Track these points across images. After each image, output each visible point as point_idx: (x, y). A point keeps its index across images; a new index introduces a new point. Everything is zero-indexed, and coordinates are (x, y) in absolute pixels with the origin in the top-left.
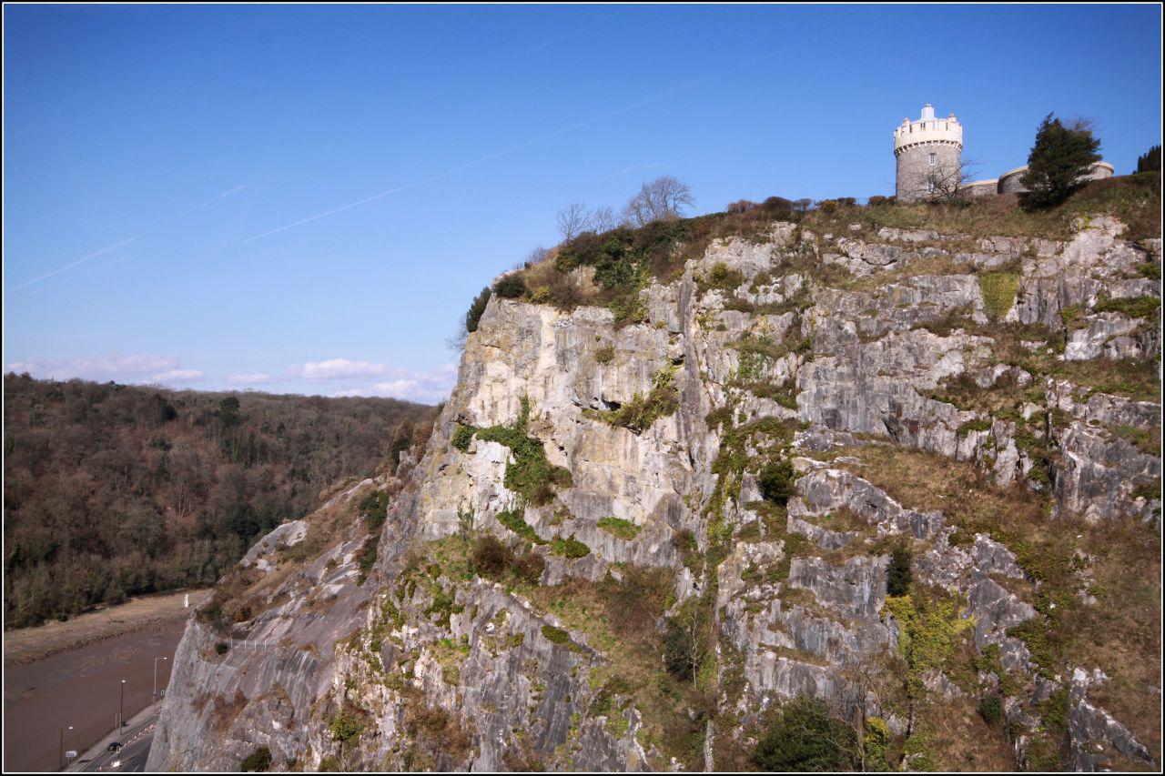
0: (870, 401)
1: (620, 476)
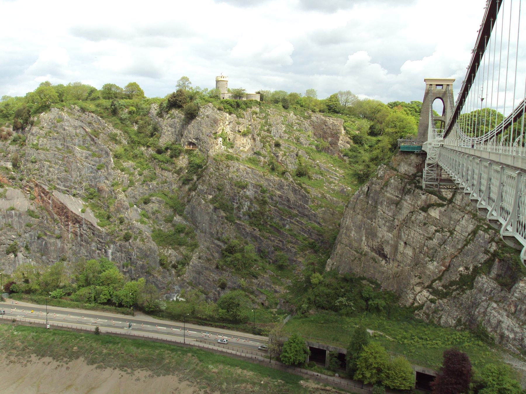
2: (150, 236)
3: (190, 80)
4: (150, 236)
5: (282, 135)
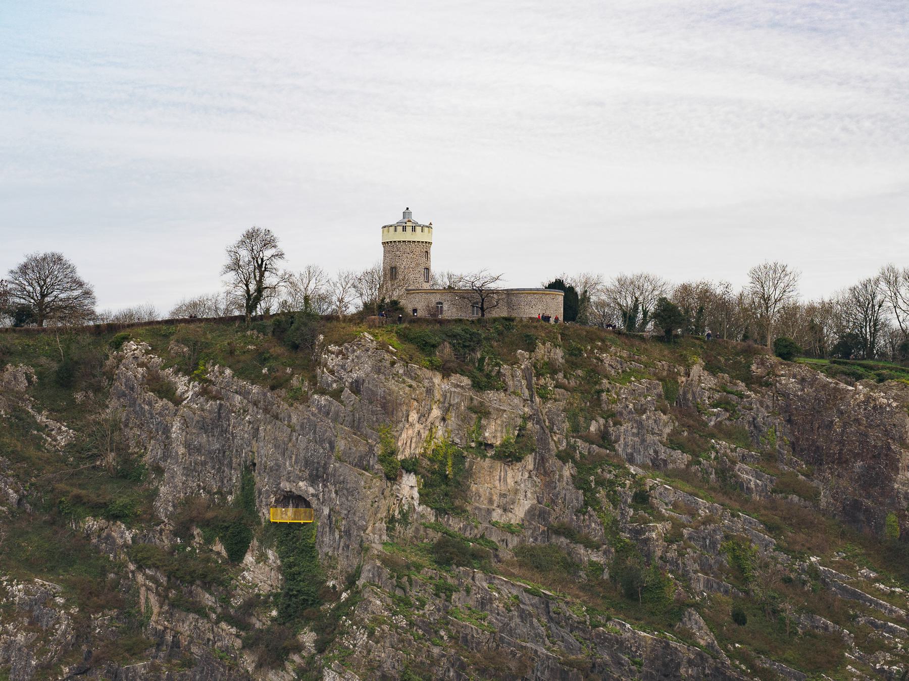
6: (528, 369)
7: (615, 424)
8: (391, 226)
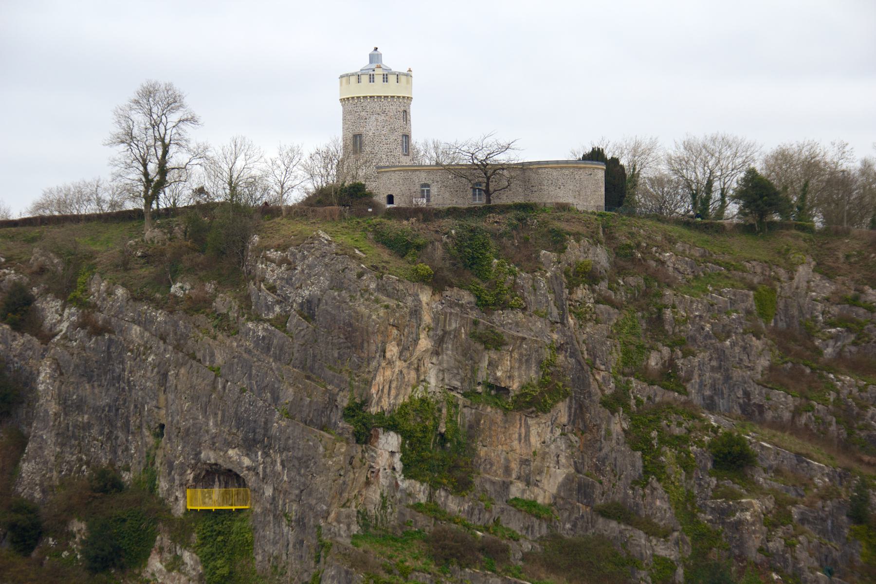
0: (732, 389)
1: (515, 460)
2: (699, 514)
3: (186, 101)
4: (699, 514)
5: (756, 399)
6: (556, 278)
7: (685, 356)
8: (353, 75)
